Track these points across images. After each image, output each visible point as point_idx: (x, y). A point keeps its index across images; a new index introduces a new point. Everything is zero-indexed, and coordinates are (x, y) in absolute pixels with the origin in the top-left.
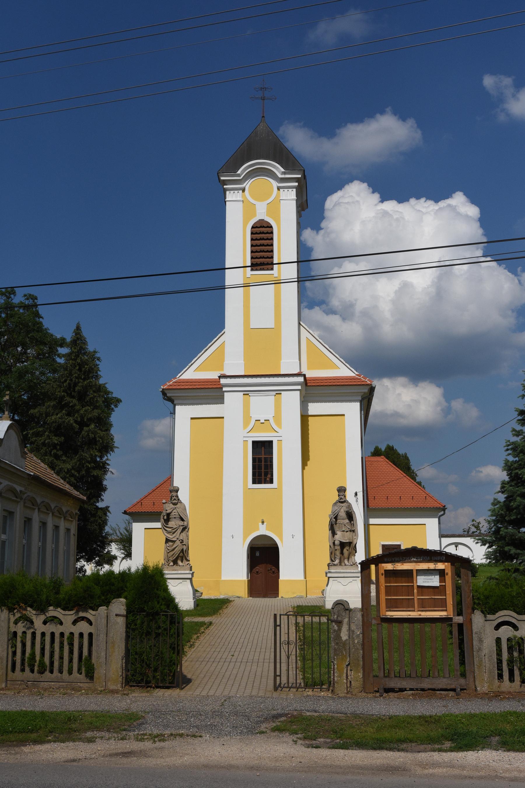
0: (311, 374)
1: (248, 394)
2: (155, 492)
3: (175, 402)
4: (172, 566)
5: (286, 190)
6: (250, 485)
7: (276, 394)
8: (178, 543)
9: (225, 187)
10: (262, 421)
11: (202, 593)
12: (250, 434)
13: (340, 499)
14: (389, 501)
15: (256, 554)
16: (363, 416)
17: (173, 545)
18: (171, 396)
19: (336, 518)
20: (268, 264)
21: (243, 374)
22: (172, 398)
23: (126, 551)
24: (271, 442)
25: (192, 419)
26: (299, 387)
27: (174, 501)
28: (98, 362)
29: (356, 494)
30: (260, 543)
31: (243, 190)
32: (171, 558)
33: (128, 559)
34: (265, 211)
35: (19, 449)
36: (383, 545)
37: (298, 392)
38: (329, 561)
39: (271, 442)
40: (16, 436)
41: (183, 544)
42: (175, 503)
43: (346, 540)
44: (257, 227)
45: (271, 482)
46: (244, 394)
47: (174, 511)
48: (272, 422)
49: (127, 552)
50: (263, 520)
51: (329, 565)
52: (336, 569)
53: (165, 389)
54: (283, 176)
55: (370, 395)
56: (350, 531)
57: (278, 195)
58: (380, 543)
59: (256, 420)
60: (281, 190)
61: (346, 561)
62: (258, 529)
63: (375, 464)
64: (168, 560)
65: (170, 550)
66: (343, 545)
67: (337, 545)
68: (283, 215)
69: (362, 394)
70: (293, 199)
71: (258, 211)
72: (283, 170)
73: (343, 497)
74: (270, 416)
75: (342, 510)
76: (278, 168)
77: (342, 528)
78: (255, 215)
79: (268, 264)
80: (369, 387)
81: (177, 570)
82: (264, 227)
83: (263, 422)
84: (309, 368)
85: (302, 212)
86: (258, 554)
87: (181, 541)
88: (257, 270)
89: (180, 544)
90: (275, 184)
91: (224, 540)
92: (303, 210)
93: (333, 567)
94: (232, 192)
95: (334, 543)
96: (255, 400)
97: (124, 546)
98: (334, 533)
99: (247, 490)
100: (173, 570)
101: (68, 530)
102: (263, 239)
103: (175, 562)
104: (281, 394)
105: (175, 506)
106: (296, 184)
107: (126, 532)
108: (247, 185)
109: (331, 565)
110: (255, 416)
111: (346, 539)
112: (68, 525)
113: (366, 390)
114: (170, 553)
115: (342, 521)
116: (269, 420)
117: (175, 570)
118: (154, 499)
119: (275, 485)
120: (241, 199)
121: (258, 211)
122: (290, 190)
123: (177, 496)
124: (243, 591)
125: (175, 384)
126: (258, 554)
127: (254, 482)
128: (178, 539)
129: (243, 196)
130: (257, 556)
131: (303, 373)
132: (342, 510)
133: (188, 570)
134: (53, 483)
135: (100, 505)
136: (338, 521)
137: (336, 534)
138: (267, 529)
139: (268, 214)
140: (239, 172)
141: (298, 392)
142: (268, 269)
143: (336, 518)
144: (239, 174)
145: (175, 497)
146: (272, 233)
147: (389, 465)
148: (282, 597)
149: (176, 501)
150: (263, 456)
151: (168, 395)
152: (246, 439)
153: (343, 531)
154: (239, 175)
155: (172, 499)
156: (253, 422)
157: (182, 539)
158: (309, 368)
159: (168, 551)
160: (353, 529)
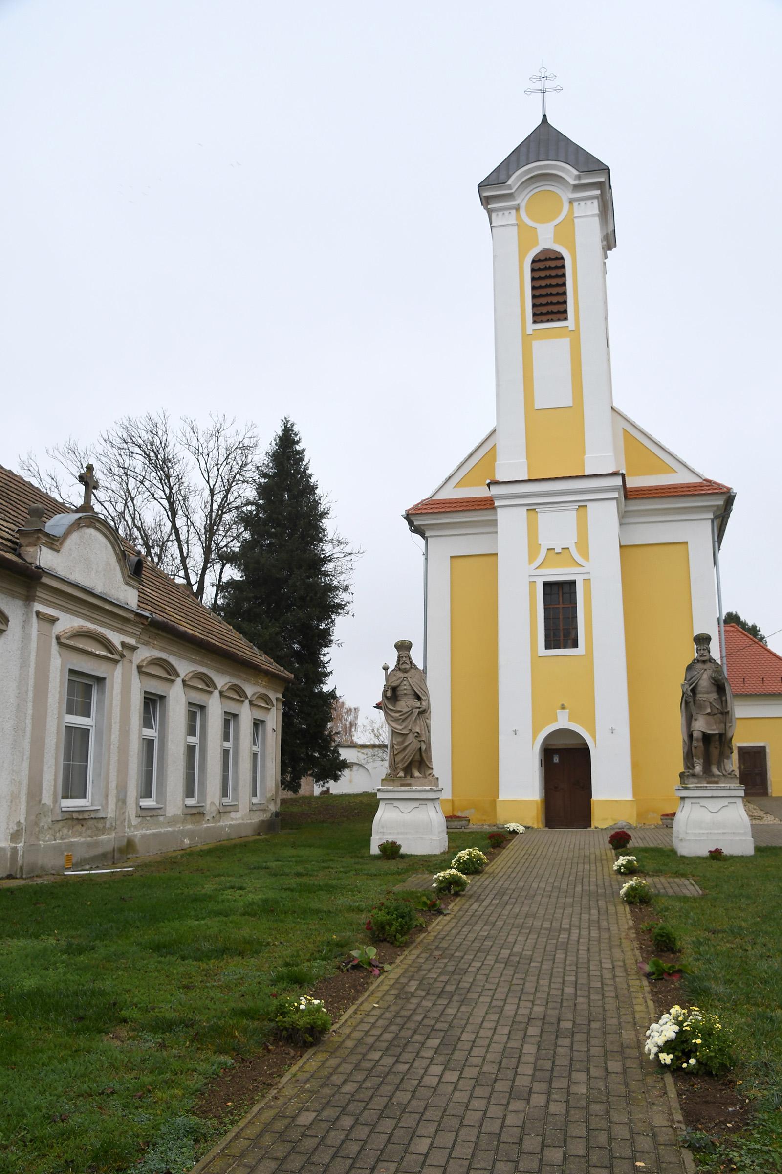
0: (631, 483)
3: (427, 535)
4: (400, 777)
5: (582, 203)
6: (542, 650)
8: (411, 737)
9: (489, 207)
10: (558, 550)
13: (701, 656)
15: (553, 760)
17: (403, 742)
18: (420, 525)
19: (693, 690)
20: (559, 312)
21: (526, 478)
22: (422, 528)
24: (573, 583)
25: (452, 557)
26: (616, 495)
27: (403, 667)
30: (561, 743)
31: (517, 208)
32: (400, 765)
34: (551, 235)
35: (118, 568)
37: (614, 503)
38: (682, 769)
39: (573, 583)
40: (109, 545)
41: (420, 739)
42: (405, 669)
44: (540, 261)
45: (575, 645)
47: (405, 683)
50: (563, 705)
51: (682, 775)
53: (411, 514)
54: (576, 182)
55: (725, 511)
57: (571, 210)
60: (575, 204)
61: (715, 771)
62: (555, 720)
64: (396, 768)
66: (707, 738)
68: (579, 239)
70: (593, 215)
71: (541, 238)
72: (576, 172)
73: (705, 653)
74: (570, 540)
76: (569, 170)
78: (536, 242)
79: (559, 312)
80: (724, 497)
82: (550, 259)
85: (608, 252)
86: (556, 759)
87: (416, 734)
88: (542, 322)
90: (566, 195)
91: (502, 738)
92: (610, 249)
93: (692, 780)
94: (500, 214)
95: (690, 736)
96: (544, 518)
98: (689, 720)
99: (535, 659)
100: (402, 785)
101: (258, 724)
102: (552, 303)
103: (408, 770)
105: (406, 675)
106: (598, 192)
108: (522, 200)
109: (688, 776)
110: (546, 542)
112: (259, 715)
113: (720, 502)
114: (398, 756)
115: (705, 695)
119: (581, 649)
120: (514, 222)
121: (540, 238)
122: (589, 202)
124: (534, 816)
125: (424, 507)
126: (556, 759)
127: (548, 647)
128: (411, 730)
129: (518, 217)
130: (556, 763)
131: (621, 472)
132: (705, 676)
134: (229, 648)
135: (326, 688)
136: (698, 695)
137: (696, 720)
139: (556, 240)
140: (509, 182)
141: (614, 503)
142: (559, 320)
143: (693, 690)
144: (510, 185)
145: (404, 659)
146: (563, 267)
148: (596, 828)
149: (408, 667)
150: (561, 606)
151: (415, 523)
154: (510, 187)
155: (401, 663)
157: (418, 731)
159: (396, 753)
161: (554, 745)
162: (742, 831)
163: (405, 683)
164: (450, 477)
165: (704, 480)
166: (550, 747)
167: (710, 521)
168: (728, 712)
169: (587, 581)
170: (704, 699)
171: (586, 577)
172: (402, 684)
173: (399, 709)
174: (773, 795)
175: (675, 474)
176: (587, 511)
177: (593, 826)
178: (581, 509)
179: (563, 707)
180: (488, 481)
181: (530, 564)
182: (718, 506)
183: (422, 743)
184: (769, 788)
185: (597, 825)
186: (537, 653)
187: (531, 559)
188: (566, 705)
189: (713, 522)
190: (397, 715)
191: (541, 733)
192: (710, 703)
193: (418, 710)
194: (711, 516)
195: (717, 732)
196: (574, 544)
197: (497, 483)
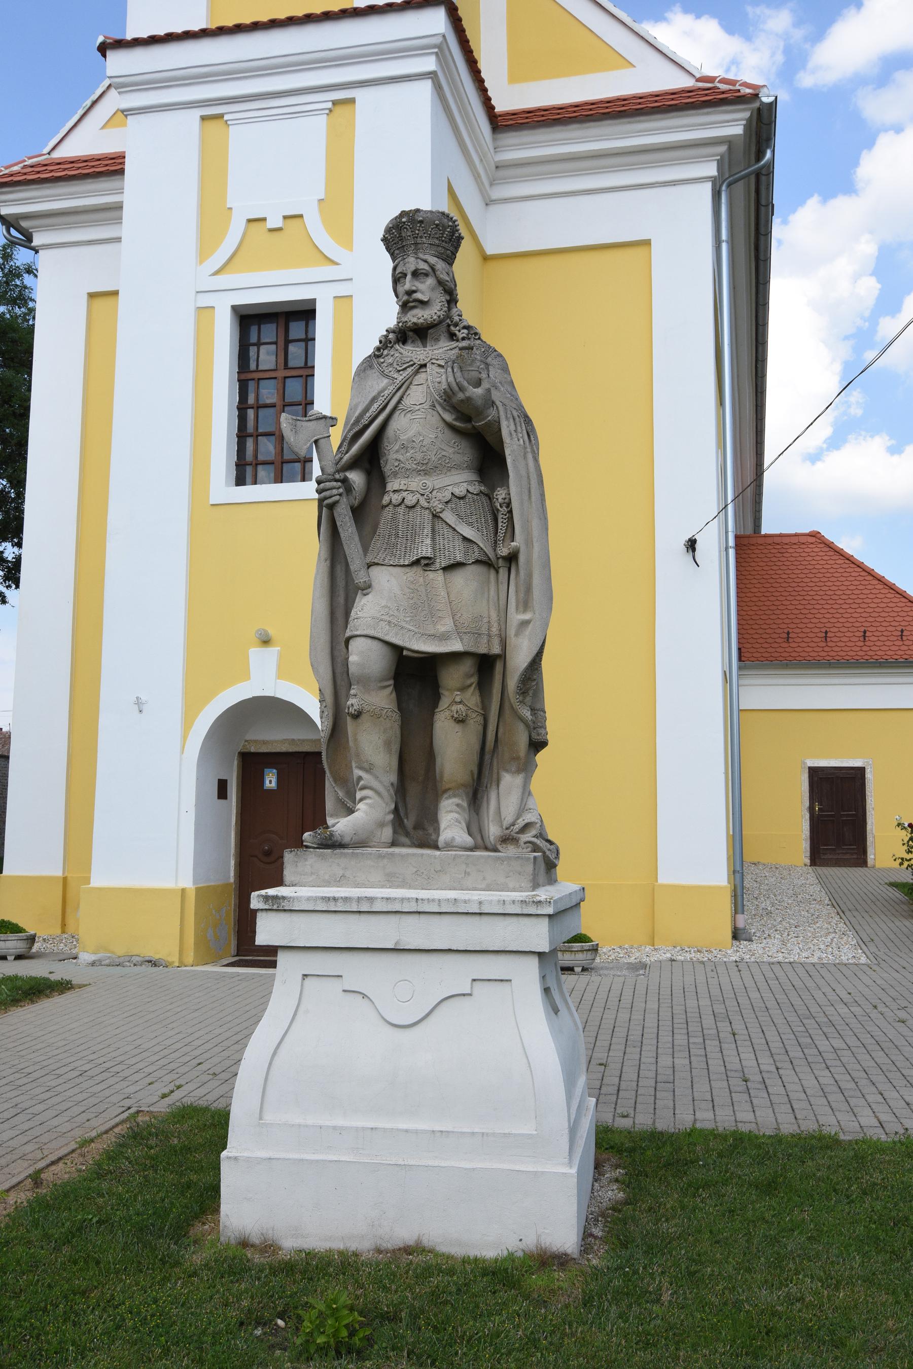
1: (221, 116)
7: (335, 103)
10: (275, 221)
11: (32, 939)
12: (224, 281)
14: (830, 644)
16: (724, 247)
25: (92, 296)
26: (429, 64)
28: (28, 280)
29: (692, 545)
36: (810, 768)
43: (444, 637)
48: (314, 223)
52: (340, 881)
56: (486, 563)
58: (804, 763)
59: (250, 221)
62: (245, 675)
63: (791, 550)
67: (364, 681)
73: (425, 289)
75: (417, 395)
77: (413, 536)
83: (279, 223)
84: (515, 76)
86: (271, 781)
104: (352, 101)
111: (445, 625)
115: (415, 483)
116: (301, 216)
126: (271, 781)
130: (270, 791)
137: (367, 588)
138: (282, 673)
141: (426, 86)
147: (832, 553)
152: (205, 301)
153: (423, 563)
156: (237, 227)
158: (515, 76)
160: (504, 551)
161: (264, 742)
162: (527, 1128)
165: (698, 80)
166: (253, 750)
167: (708, 186)
168: (512, 558)
170: (410, 500)
171: (342, 289)
174: (877, 866)
175: (628, 71)
178: (339, 110)
179: (266, 641)
180: (101, 39)
182: (728, 141)
184: (870, 850)
187: (203, 253)
188: (271, 632)
189: (716, 195)
191: (207, 708)
192: (436, 516)
194: (711, 170)
195: (456, 646)
196: (316, 202)
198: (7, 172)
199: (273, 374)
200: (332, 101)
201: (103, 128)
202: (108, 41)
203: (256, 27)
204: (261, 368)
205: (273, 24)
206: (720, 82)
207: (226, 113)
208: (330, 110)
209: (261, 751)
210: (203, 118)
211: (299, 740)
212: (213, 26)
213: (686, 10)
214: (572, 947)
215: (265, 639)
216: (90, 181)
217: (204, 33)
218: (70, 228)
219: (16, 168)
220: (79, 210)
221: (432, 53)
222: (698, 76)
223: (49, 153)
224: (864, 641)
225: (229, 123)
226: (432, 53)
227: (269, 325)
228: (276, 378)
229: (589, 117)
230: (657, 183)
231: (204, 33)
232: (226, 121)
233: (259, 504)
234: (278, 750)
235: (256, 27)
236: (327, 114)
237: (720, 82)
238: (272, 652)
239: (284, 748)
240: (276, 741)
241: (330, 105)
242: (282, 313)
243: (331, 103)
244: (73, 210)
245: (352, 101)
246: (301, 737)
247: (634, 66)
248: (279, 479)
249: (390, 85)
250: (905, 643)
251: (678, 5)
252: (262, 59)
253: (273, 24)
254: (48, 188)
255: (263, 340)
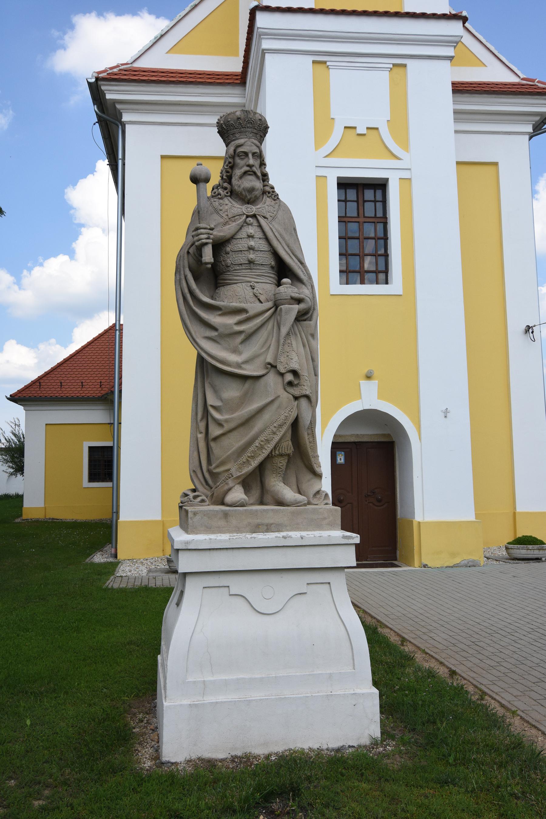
1: (325, 62)
2: (59, 370)
7: (394, 65)
10: (361, 130)
17: (244, 399)
22: (118, 106)
23: (15, 463)
33: (19, 475)
41: (296, 392)
46: (314, 62)
49: (17, 465)
53: (104, 79)
59: (345, 127)
62: (358, 396)
65: (227, 427)
69: (537, 118)
81: (279, 528)
83: (365, 131)
87: (289, 377)
89: (285, 396)
97: (13, 457)
100: (256, 528)
104: (405, 66)
105: (253, 209)
107: (14, 438)
116: (377, 129)
117: (268, 528)
118: (61, 378)
123: (260, 156)
130: (341, 465)
133: (331, 526)
138: (381, 396)
148: (425, 566)
155: (238, 172)
157: (294, 365)
163: (251, 230)
164: (162, 36)
165: (523, 79)
169: (406, 182)
171: (405, 175)
172: (243, 234)
173: (235, 304)
175: (485, 67)
176: (406, 75)
177: (416, 563)
178: (396, 70)
179: (369, 377)
180: (255, 3)
181: (316, 149)
183: (304, 402)
185: (425, 562)
186: (329, 289)
187: (319, 143)
188: (376, 374)
190: (231, 320)
191: (335, 416)
193: (296, 308)
197: (268, 9)
198: (111, 71)
199: (357, 220)
200: (393, 64)
201: (167, 53)
202: (261, 6)
203: (375, 14)
204: (348, 215)
205: (365, 13)
206: (538, 82)
207: (328, 61)
208: (391, 69)
209: (338, 441)
210: (314, 62)
211: (361, 435)
212: (318, 7)
213: (150, 13)
214: (543, 547)
215: (369, 376)
216: (173, 85)
217: (311, 11)
218: (149, 113)
219: (115, 70)
220: (180, 103)
221: (452, 46)
222: (522, 77)
223: (131, 63)
224: (40, 388)
225: (329, 67)
226: (452, 46)
227: (352, 190)
228: (359, 222)
229: (477, 92)
230: (502, 132)
231: (311, 11)
232: (328, 66)
233: (361, 296)
234: (349, 441)
235: (375, 14)
236: (389, 71)
237: (538, 82)
238: (373, 385)
239: (352, 440)
240: (347, 436)
241: (391, 66)
242: (361, 184)
243: (392, 65)
244: (155, 102)
245: (405, 66)
246: (362, 433)
247: (486, 66)
248: (362, 282)
249: (409, 59)
250: (104, 389)
251: (146, 8)
252: (355, 33)
253: (365, 13)
254: (142, 86)
255: (348, 199)
